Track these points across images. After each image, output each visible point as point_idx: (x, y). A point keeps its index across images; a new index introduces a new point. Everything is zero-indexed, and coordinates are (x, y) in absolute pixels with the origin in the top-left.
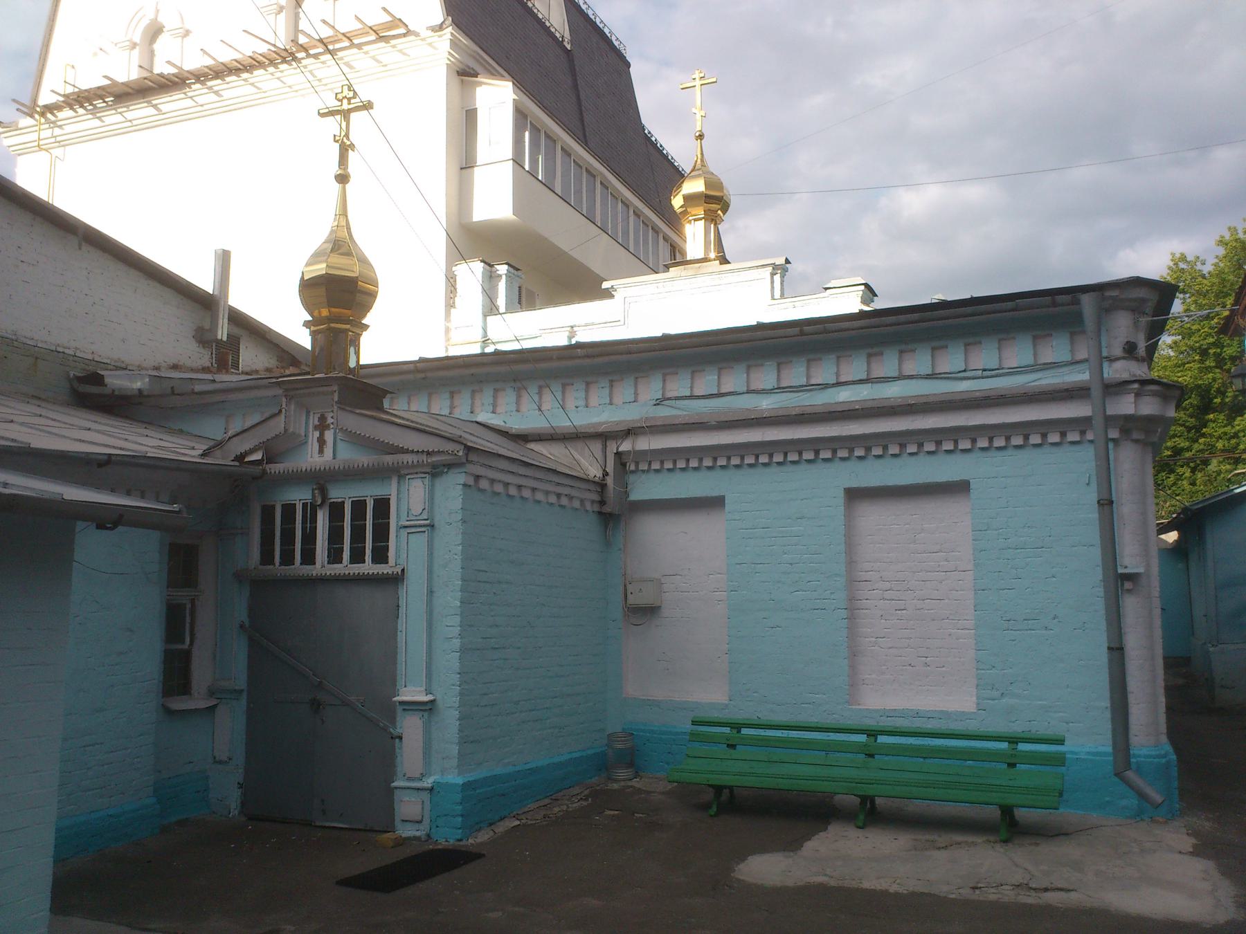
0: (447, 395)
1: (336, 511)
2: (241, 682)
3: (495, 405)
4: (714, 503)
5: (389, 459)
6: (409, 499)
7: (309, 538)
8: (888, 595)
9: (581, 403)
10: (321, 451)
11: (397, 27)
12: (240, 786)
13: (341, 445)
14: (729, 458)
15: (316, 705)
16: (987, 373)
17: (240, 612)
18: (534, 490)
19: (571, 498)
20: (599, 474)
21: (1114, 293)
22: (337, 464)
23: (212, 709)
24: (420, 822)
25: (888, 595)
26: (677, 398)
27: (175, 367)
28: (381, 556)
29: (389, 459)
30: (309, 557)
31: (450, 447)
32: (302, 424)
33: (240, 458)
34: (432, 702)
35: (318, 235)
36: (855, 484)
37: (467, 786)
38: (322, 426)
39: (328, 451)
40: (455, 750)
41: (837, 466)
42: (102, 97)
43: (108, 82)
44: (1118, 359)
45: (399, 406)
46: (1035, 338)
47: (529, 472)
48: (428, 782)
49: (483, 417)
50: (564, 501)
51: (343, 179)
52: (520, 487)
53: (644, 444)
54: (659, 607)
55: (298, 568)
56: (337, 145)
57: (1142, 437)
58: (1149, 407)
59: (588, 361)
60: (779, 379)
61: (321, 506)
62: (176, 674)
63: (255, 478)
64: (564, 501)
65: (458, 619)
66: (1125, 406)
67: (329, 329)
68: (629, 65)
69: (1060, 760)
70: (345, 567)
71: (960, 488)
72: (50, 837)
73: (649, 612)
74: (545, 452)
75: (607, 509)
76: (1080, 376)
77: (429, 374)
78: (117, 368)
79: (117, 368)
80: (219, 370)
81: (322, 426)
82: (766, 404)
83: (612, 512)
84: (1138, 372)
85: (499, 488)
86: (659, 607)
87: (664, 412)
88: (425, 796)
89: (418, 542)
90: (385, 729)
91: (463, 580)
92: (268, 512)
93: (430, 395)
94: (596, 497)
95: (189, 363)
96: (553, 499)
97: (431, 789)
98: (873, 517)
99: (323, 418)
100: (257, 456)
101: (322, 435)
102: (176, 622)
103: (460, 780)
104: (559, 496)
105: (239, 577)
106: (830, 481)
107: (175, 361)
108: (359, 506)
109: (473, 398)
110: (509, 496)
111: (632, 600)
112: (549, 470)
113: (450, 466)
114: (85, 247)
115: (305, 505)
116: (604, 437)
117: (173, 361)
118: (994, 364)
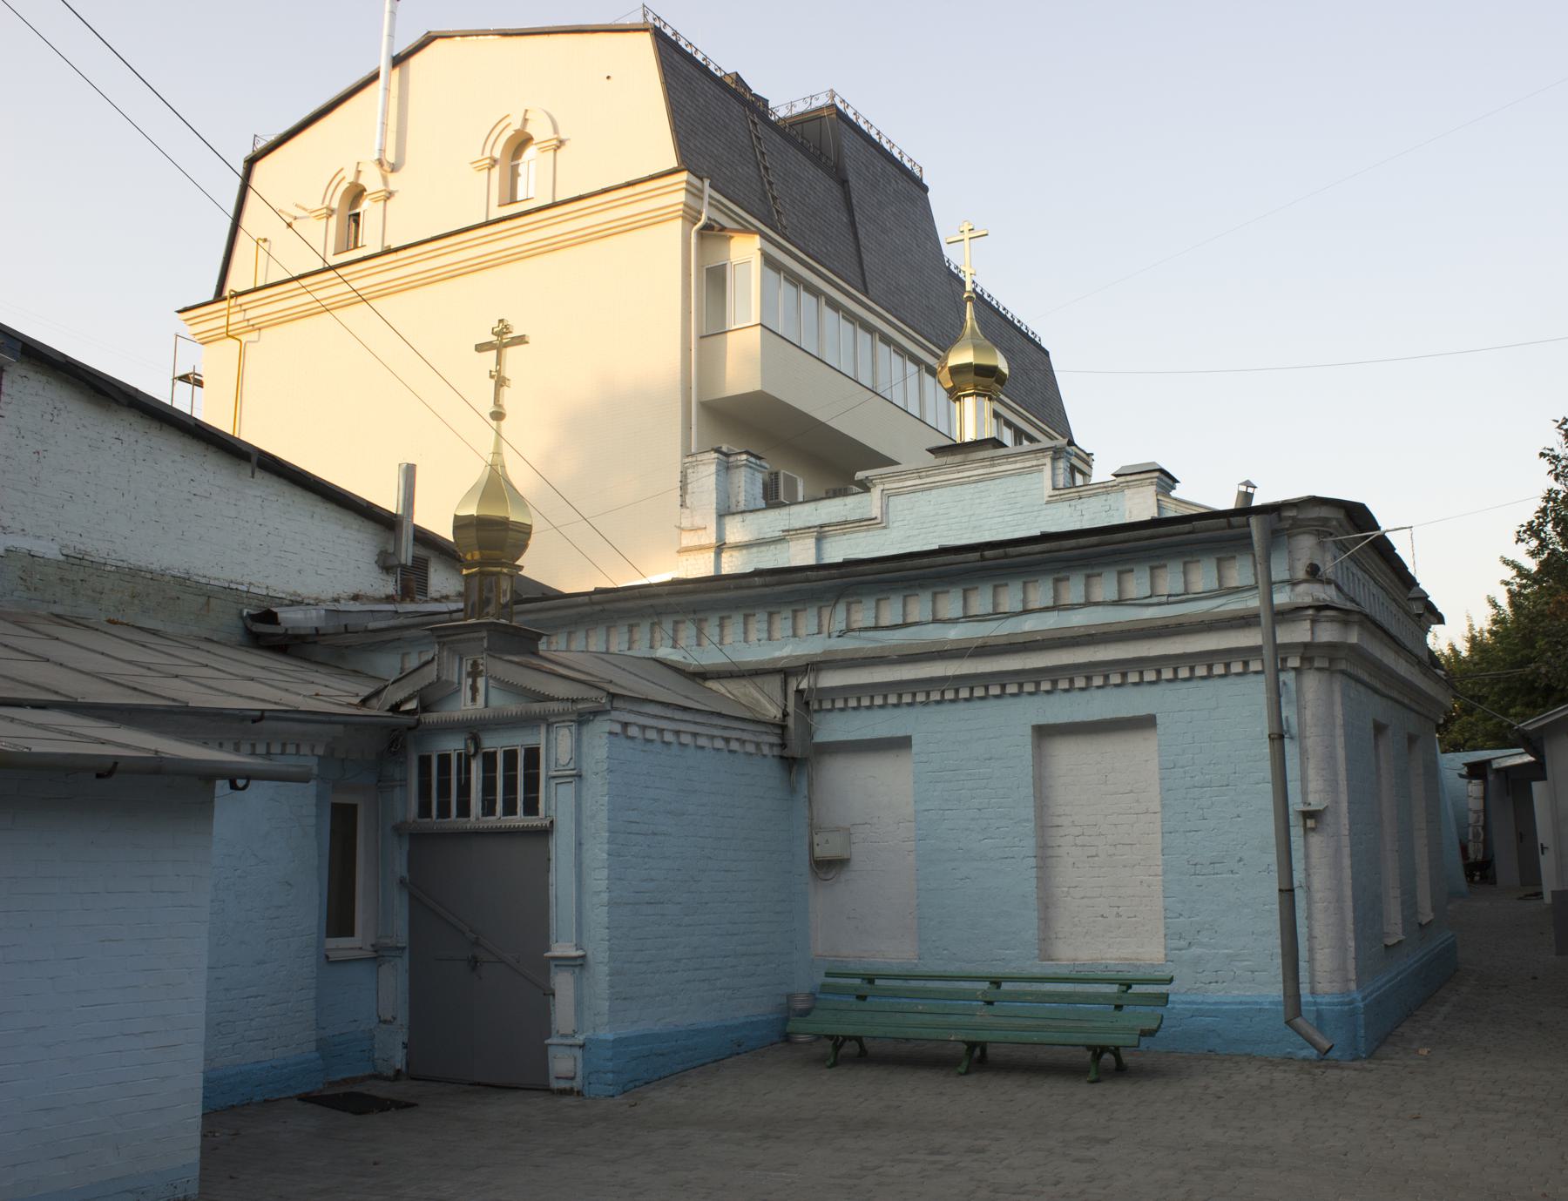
0: (626, 629)
2: (403, 938)
5: (537, 707)
6: (559, 747)
7: (465, 789)
8: (1079, 841)
10: (474, 699)
12: (405, 1046)
13: (492, 692)
14: (914, 695)
15: (474, 963)
16: (1173, 599)
17: (400, 867)
18: (695, 735)
19: (742, 742)
20: (779, 715)
22: (488, 713)
24: (573, 1078)
25: (1079, 841)
26: (860, 630)
27: (356, 598)
28: (531, 808)
29: (537, 707)
30: (464, 810)
31: (593, 693)
32: (455, 671)
33: (395, 708)
34: (583, 957)
35: (476, 472)
36: (1042, 721)
37: (618, 1042)
38: (475, 674)
40: (605, 1005)
41: (1025, 701)
45: (555, 646)
47: (687, 716)
48: (580, 1039)
49: (664, 652)
50: (734, 746)
51: (498, 416)
52: (677, 733)
53: (830, 680)
54: (848, 860)
56: (493, 382)
57: (1326, 665)
58: (1328, 633)
59: (767, 590)
60: (965, 606)
61: (474, 755)
63: (410, 729)
64: (734, 746)
65: (606, 872)
66: (1299, 633)
67: (481, 573)
68: (925, 189)
69: (1164, 999)
70: (499, 820)
71: (1146, 723)
72: (199, 1083)
73: (828, 867)
74: (723, 690)
75: (787, 753)
76: (1253, 602)
77: (607, 606)
78: (293, 603)
79: (293, 603)
80: (403, 600)
81: (475, 674)
82: (954, 634)
83: (796, 755)
84: (1322, 596)
85: (652, 735)
86: (848, 860)
87: (849, 644)
88: (578, 1053)
89: (566, 793)
91: (610, 831)
92: (425, 762)
93: (608, 629)
94: (775, 740)
95: (370, 592)
96: (719, 744)
97: (582, 1046)
98: (1068, 756)
99: (475, 664)
100: (412, 705)
101: (474, 682)
103: (611, 1037)
104: (727, 740)
105: (398, 830)
107: (355, 591)
108: (510, 756)
109: (652, 632)
110: (681, 744)
111: (820, 852)
112: (712, 713)
113: (595, 713)
114: (259, 474)
115: (459, 755)
116: (785, 672)
117: (353, 590)
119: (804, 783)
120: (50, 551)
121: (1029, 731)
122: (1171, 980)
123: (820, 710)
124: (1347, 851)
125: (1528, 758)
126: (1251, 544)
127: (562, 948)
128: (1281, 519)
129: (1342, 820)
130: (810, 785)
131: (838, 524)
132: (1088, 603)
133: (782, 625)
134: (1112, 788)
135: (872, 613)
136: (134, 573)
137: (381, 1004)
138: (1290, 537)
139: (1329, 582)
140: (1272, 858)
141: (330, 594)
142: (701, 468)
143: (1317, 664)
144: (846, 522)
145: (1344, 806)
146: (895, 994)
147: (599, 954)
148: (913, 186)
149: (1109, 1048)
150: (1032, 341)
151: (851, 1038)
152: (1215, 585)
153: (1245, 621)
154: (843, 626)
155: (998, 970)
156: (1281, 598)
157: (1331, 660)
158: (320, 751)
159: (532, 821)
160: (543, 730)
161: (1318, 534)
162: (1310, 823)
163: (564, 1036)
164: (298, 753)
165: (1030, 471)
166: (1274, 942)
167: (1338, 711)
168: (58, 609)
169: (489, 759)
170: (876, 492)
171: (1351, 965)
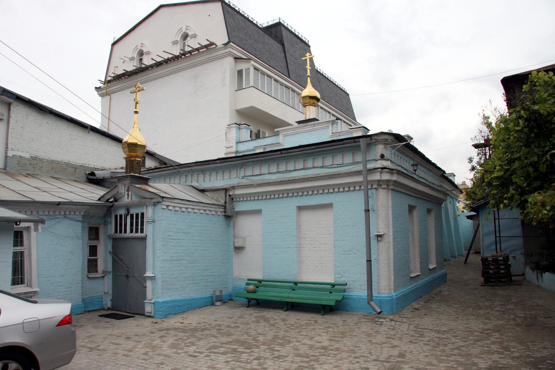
1: (132, 216)
2: (111, 270)
3: (198, 180)
4: (259, 212)
6: (149, 213)
9: (222, 178)
10: (128, 198)
11: (213, 45)
12: (111, 300)
13: (133, 196)
16: (339, 166)
17: (110, 248)
20: (223, 202)
21: (376, 137)
23: (104, 277)
28: (142, 231)
30: (125, 232)
33: (107, 201)
36: (300, 205)
39: (130, 198)
41: (294, 199)
42: (124, 76)
43: (124, 72)
44: (378, 160)
46: (353, 153)
48: (153, 301)
49: (195, 184)
53: (238, 192)
55: (123, 235)
58: (386, 176)
59: (220, 164)
60: (286, 168)
62: (92, 265)
64: (208, 212)
66: (377, 176)
68: (309, 47)
70: (134, 235)
71: (329, 206)
73: (239, 249)
75: (226, 214)
76: (359, 167)
82: (274, 178)
85: (177, 209)
87: (245, 181)
88: (152, 305)
90: (143, 284)
92: (116, 216)
94: (223, 210)
96: (202, 211)
98: (307, 216)
100: (111, 200)
102: (93, 250)
104: (205, 210)
105: (109, 237)
106: (290, 205)
108: (137, 215)
111: (236, 245)
114: (91, 133)
118: (340, 162)
119: (232, 223)
120: (27, 156)
121: (295, 208)
122: (346, 284)
123: (237, 201)
124: (392, 248)
125: (475, 213)
126: (360, 149)
127: (148, 274)
128: (371, 139)
129: (389, 238)
130: (234, 224)
131: (270, 145)
132: (314, 167)
133: (227, 175)
134: (318, 225)
135: (251, 171)
136: (53, 162)
137: (104, 288)
138: (375, 145)
139: (388, 160)
140: (365, 250)
141: (113, 167)
142: (232, 129)
143: (383, 187)
144: (272, 144)
145: (391, 233)
146: (265, 286)
147: (158, 276)
148: (306, 46)
149: (327, 305)
150: (344, 91)
151: (254, 299)
152: (352, 161)
153: (358, 173)
154: (243, 175)
155: (296, 281)
156: (370, 166)
157: (388, 186)
158: (82, 214)
159: (142, 235)
160: (145, 207)
161: (385, 144)
162: (379, 239)
163: (149, 300)
164: (75, 214)
165: (325, 128)
166: (365, 277)
167: (390, 202)
168: (28, 172)
169: (132, 216)
170: (281, 135)
171: (392, 284)
